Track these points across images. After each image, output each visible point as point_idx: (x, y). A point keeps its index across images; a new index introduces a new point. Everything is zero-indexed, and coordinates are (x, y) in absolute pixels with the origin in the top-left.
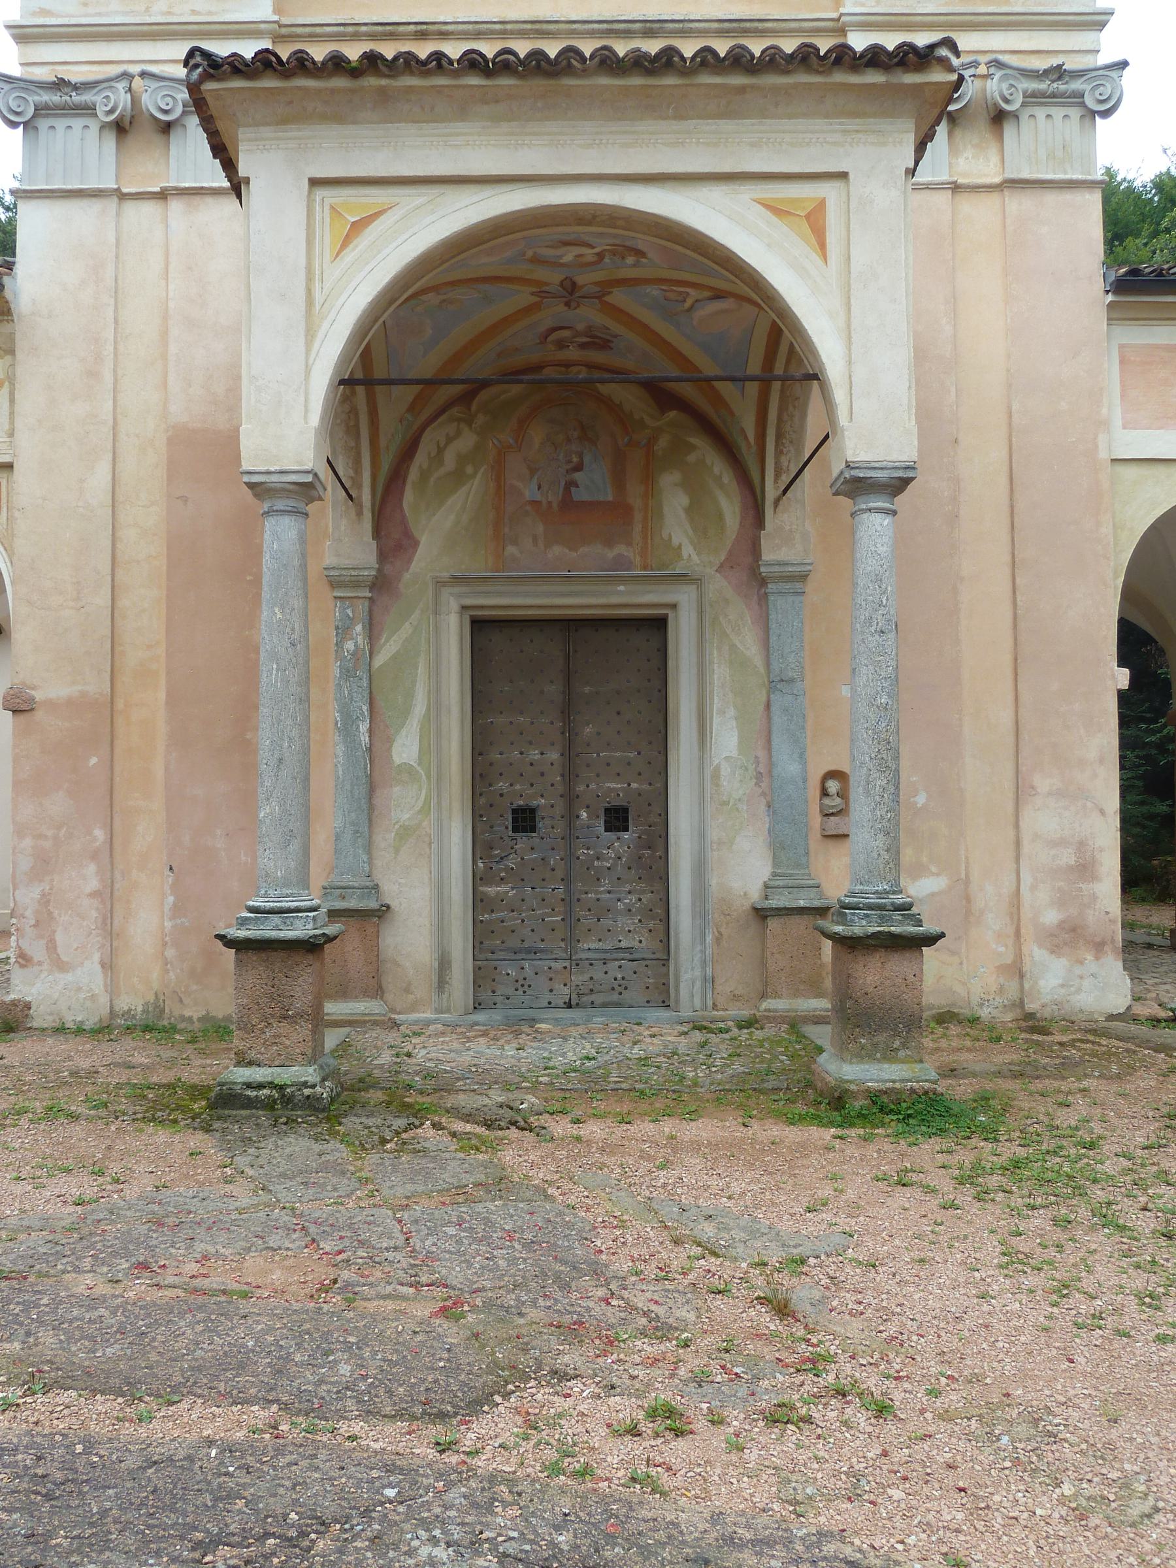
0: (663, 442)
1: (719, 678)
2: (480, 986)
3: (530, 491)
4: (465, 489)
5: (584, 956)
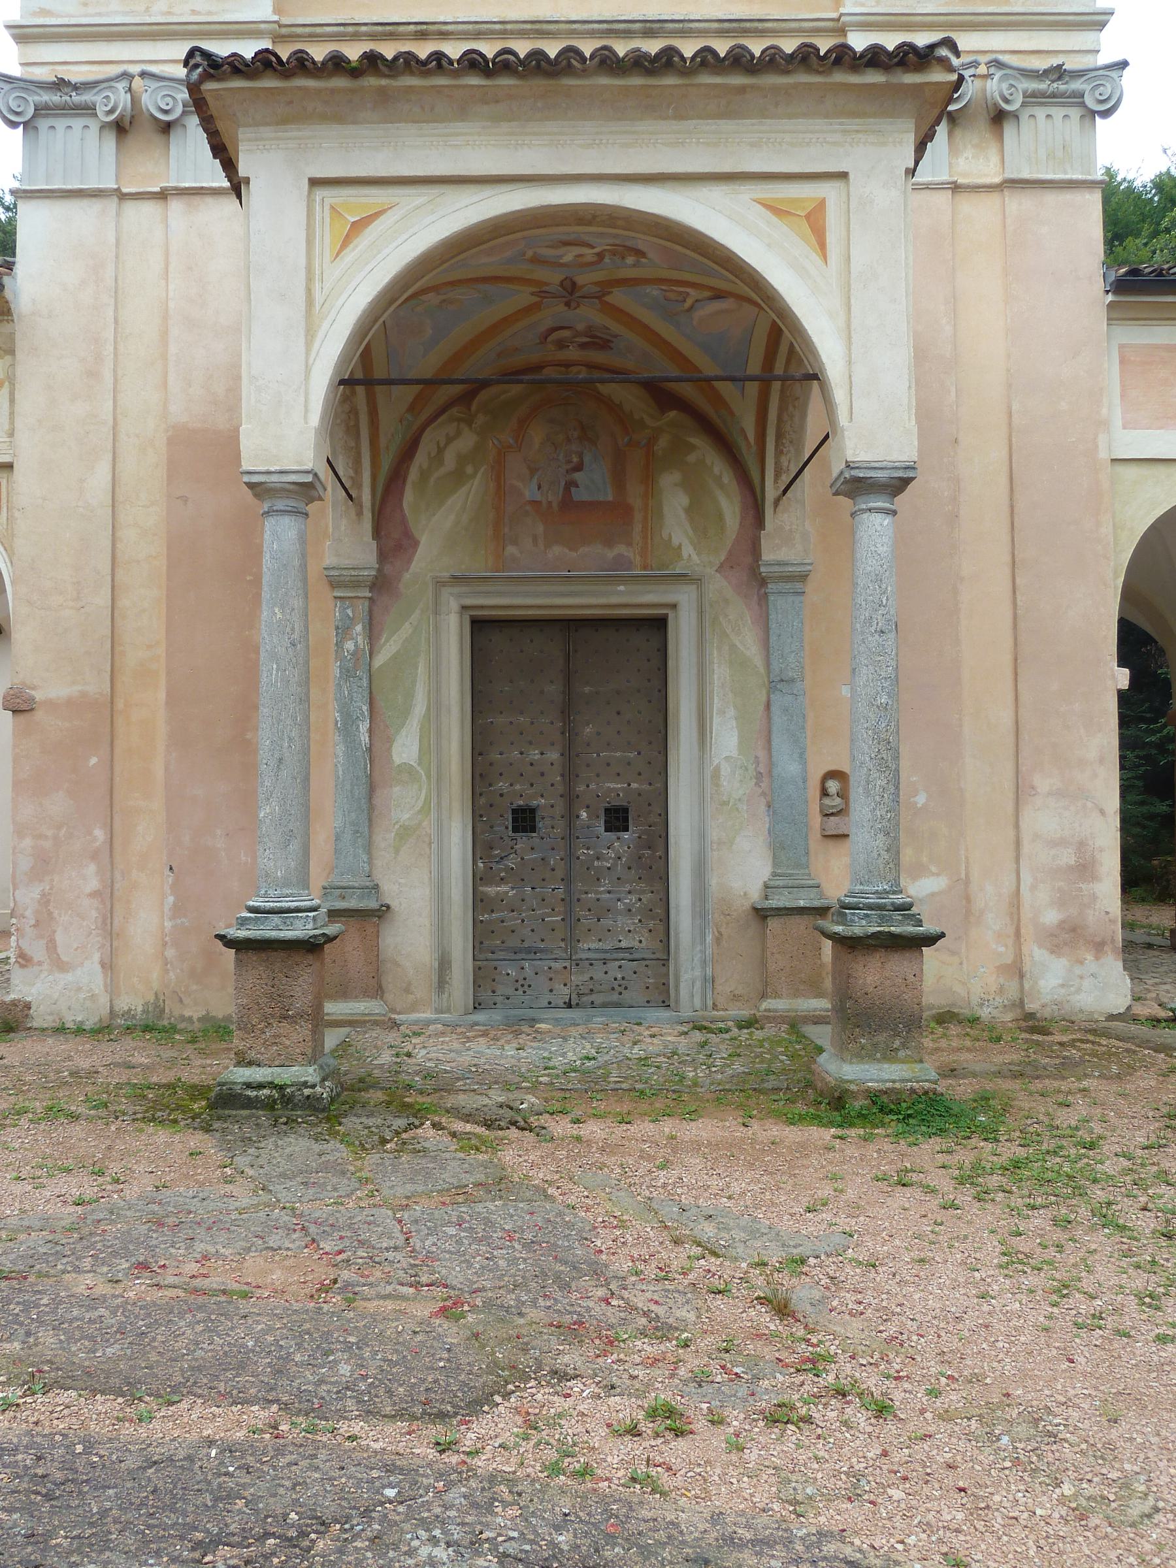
0: (663, 442)
1: (719, 678)
2: (480, 986)
3: (530, 491)
4: (465, 489)
5: (584, 956)
